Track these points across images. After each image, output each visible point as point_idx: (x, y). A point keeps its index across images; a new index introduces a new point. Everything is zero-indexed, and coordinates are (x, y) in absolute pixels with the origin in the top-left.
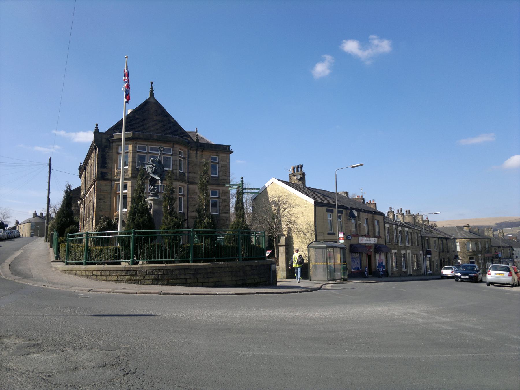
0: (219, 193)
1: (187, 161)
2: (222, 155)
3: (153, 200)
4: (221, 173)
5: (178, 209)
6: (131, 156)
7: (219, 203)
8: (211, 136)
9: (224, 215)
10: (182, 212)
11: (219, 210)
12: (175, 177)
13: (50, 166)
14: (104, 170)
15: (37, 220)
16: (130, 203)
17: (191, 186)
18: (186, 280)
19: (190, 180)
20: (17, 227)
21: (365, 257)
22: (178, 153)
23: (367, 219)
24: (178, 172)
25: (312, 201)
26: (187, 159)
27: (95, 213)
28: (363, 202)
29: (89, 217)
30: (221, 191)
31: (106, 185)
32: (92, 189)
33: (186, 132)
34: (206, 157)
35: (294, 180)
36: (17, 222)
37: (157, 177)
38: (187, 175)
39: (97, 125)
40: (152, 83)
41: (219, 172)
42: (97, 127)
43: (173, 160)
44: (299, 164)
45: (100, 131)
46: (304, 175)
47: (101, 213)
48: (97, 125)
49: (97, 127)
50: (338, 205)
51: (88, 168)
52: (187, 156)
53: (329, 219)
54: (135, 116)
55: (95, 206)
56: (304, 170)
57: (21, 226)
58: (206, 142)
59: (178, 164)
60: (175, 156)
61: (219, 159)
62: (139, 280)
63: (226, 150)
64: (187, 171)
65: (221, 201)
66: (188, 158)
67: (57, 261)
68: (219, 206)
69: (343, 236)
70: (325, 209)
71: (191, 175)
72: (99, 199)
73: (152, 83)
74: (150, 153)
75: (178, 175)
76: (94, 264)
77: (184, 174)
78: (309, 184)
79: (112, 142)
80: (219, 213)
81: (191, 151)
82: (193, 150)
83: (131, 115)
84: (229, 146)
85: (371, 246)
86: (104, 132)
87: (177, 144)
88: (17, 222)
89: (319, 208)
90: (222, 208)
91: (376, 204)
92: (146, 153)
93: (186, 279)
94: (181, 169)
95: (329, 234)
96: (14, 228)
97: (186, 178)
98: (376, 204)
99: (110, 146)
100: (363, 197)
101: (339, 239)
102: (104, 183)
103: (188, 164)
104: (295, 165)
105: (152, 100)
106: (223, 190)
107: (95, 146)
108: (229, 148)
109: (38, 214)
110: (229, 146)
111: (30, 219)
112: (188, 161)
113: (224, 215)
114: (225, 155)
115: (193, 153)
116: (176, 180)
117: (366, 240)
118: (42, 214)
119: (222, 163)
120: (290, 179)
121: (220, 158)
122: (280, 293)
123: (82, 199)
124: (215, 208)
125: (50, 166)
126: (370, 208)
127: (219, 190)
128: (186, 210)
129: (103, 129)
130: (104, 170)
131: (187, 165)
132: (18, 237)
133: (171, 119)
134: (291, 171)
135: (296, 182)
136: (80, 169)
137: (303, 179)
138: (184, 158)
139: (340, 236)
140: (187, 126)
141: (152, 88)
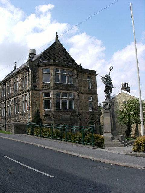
0: (92, 99)
2: (92, 76)
14: (35, 84)
16: (141, 120)
31: (36, 93)
34: (85, 78)
41: (91, 86)
46: (129, 88)
60: (70, 78)
61: (91, 78)
73: (57, 33)
74: (62, 74)
79: (39, 67)
81: (79, 74)
119: (93, 81)
121: (92, 78)
127: (92, 96)
130: (35, 84)
141: (15, 65)
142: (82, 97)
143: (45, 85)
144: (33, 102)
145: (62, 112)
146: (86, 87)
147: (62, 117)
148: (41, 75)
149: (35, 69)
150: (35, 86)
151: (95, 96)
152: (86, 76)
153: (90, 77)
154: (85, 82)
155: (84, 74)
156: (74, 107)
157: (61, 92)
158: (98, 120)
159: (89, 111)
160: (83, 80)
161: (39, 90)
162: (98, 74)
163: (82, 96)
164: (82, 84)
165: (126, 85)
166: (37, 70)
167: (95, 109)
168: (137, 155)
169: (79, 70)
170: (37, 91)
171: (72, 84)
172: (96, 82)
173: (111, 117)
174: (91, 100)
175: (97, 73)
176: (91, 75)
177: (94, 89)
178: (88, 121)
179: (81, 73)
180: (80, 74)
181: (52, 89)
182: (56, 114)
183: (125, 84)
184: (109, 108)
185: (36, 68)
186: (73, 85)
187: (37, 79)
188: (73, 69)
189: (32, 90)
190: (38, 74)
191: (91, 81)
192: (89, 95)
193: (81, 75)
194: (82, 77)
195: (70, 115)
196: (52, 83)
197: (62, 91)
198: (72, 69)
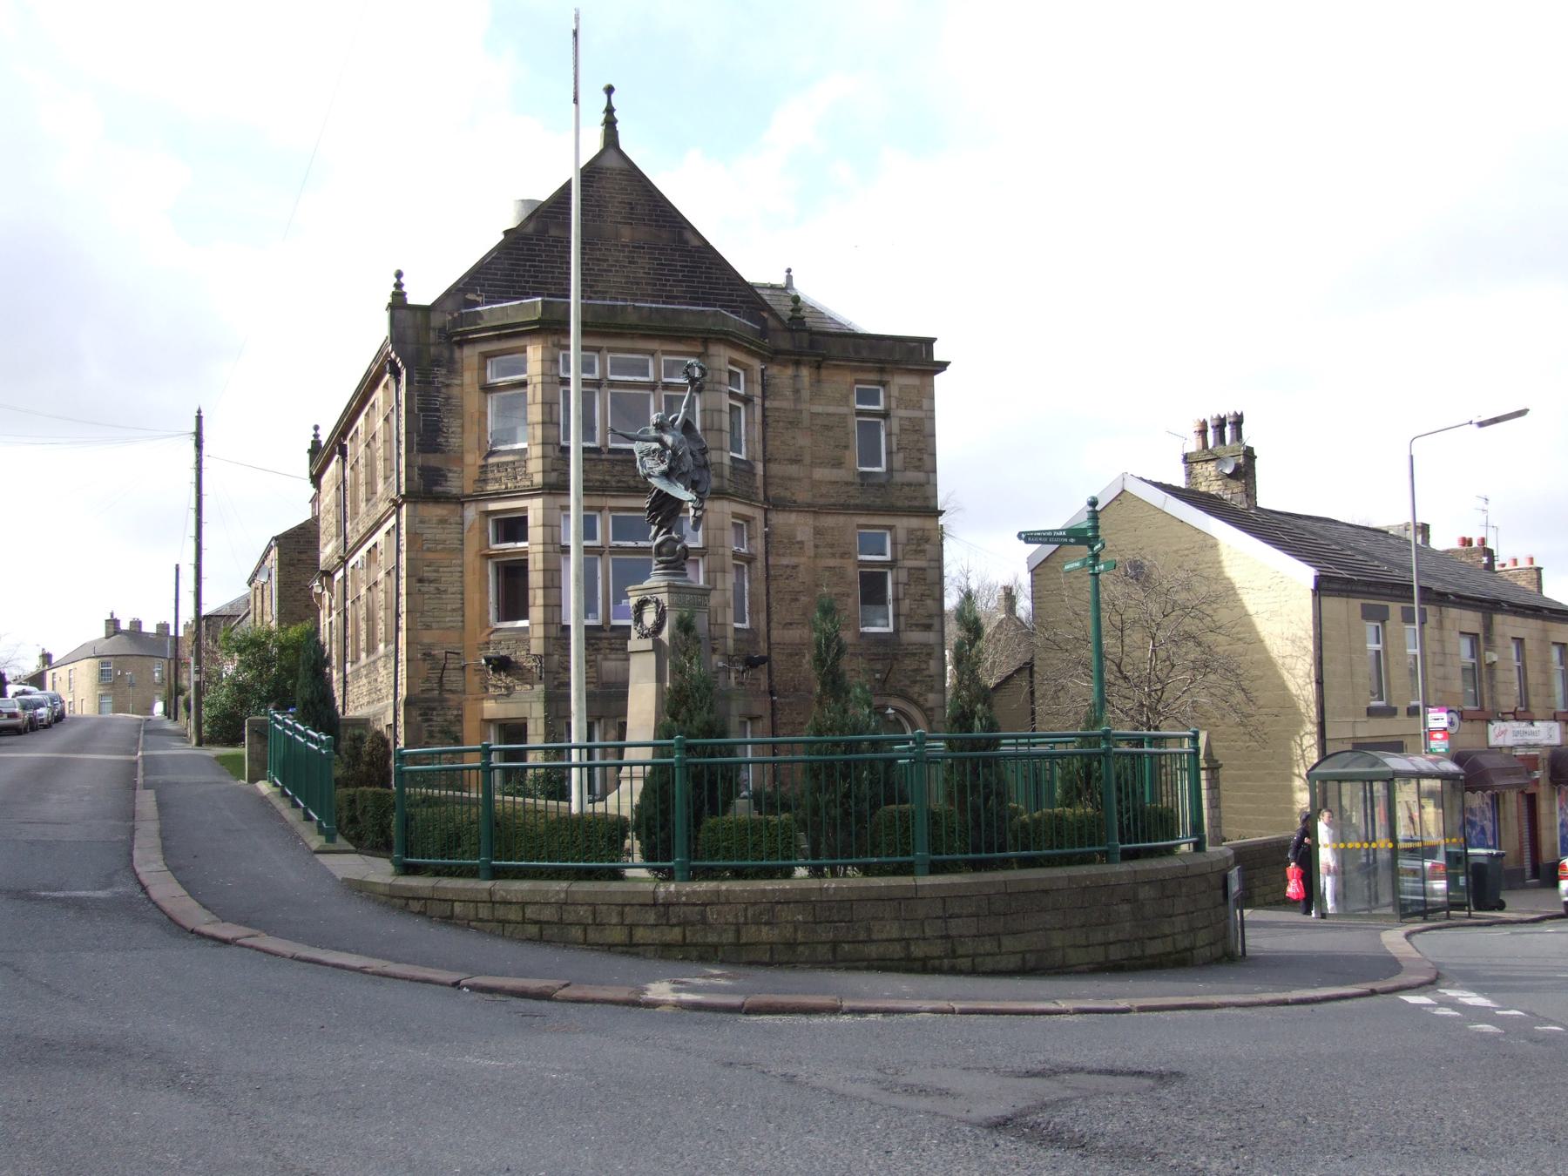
0: (894, 544)
2: (899, 381)
3: (672, 589)
4: (898, 460)
5: (730, 613)
6: (539, 398)
7: (896, 584)
8: (861, 304)
9: (916, 636)
10: (747, 625)
11: (896, 616)
12: (714, 483)
13: (199, 445)
14: (434, 460)
15: (121, 646)
16: (540, 593)
17: (778, 519)
18: (907, 947)
19: (772, 492)
20: (49, 674)
21: (1513, 806)
22: (725, 377)
23: (1520, 641)
24: (727, 461)
25: (1303, 575)
26: (758, 401)
27: (403, 635)
28: (1490, 566)
29: (371, 649)
30: (902, 536)
31: (443, 521)
32: (380, 536)
33: (751, 288)
34: (839, 395)
35: (1210, 480)
36: (47, 658)
37: (680, 492)
38: (759, 468)
39: (399, 275)
40: (609, 90)
41: (889, 453)
42: (399, 285)
43: (703, 411)
44: (1227, 410)
45: (409, 302)
46: (1250, 455)
47: (427, 637)
48: (399, 275)
49: (399, 285)
50: (1421, 588)
51: (356, 448)
52: (758, 390)
53: (1373, 646)
54: (547, 231)
55: (403, 608)
56: (1250, 437)
57: (62, 672)
58: (832, 328)
59: (726, 425)
60: (723, 400)
61: (888, 397)
62: (715, 947)
63: (913, 359)
64: (759, 455)
65: (903, 575)
66: (764, 397)
67: (331, 847)
68: (896, 600)
69: (1444, 724)
70: (1356, 604)
71: (775, 468)
72: (416, 578)
73: (609, 90)
74: (612, 384)
75: (727, 472)
76: (521, 874)
77: (749, 464)
78: (1272, 494)
79: (460, 344)
80: (897, 630)
81: (774, 370)
82: (784, 364)
83: (531, 228)
84: (929, 342)
85: (1535, 758)
86: (428, 301)
87: (719, 341)
88: (47, 658)
89: (1332, 604)
90: (906, 605)
91: (1539, 570)
92: (652, 387)
93: (908, 941)
94: (736, 447)
95: (1371, 712)
96: (37, 680)
97: (759, 482)
98: (1539, 570)
99: (452, 361)
100: (1489, 545)
101: (1430, 734)
102: (435, 511)
103: (765, 424)
104: (1210, 414)
105: (611, 161)
106: (910, 531)
107: (393, 363)
108: (930, 352)
109: (125, 626)
110: (929, 342)
111: (93, 644)
113: (916, 636)
114: (912, 381)
115: (782, 375)
116: (720, 494)
117: (1516, 734)
118: (137, 624)
119: (903, 413)
120: (1189, 474)
121: (895, 391)
122: (1286, 1003)
123: (329, 574)
124: (880, 609)
125: (199, 445)
126: (1515, 587)
127: (890, 528)
128: (763, 616)
129: (423, 293)
130: (434, 460)
131: (758, 429)
132: (59, 718)
133: (688, 235)
134: (1193, 445)
135: (1215, 488)
136: (315, 449)
137: (1245, 471)
138: (747, 400)
139: (1432, 724)
140: (755, 265)
141: (610, 110)
144: (421, 581)
145: (605, 644)
146: (838, 464)
147: (605, 679)
148: (470, 398)
149: (437, 362)
151: (915, 522)
152: (840, 382)
153: (883, 384)
154: (829, 426)
155: (824, 372)
157: (600, 509)
158: (931, 696)
159: (864, 634)
160: (814, 415)
161: (460, 501)
162: (943, 366)
163: (800, 526)
165: (1228, 430)
166: (452, 368)
167: (908, 616)
169: (789, 335)
170: (452, 507)
172: (933, 418)
173: (660, 678)
174: (888, 557)
175: (938, 356)
176: (882, 370)
177: (913, 476)
179: (797, 364)
180: (790, 371)
181: (532, 493)
182: (556, 657)
183: (1220, 424)
184: (659, 626)
185: (446, 354)
187: (453, 425)
189: (406, 498)
190: (455, 391)
191: (885, 415)
192: (863, 520)
193: (796, 377)
194: (806, 394)
196: (536, 451)
197: (613, 503)
198: (700, 349)
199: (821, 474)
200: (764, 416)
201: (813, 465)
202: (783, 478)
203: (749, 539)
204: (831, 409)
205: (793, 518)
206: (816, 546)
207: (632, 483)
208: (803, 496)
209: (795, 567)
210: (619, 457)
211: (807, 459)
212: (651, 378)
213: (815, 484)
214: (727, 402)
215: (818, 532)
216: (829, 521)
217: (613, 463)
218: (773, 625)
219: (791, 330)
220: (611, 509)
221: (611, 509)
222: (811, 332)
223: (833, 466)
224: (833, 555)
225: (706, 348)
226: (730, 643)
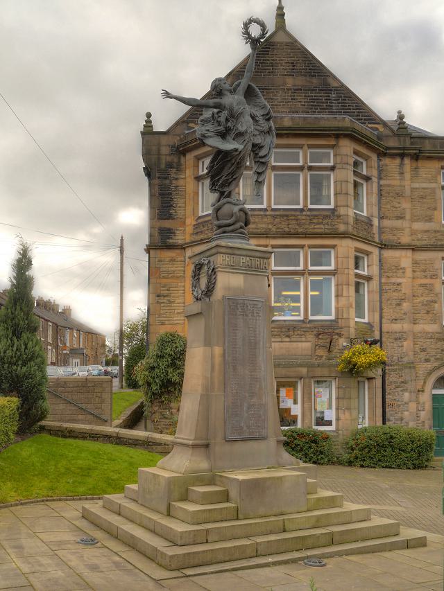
1: (375, 186)
5: (352, 312)
14: (167, 224)
17: (388, 254)
31: (172, 260)
38: (376, 222)
64: (376, 212)
66: (380, 178)
75: (351, 221)
87: (346, 136)
92: (301, 169)
103: (380, 195)
112: (380, 186)
127: (334, 247)
130: (167, 224)
133: (330, 80)
138: (367, 179)
142: (403, 265)
143: (202, 223)
150: (169, 229)
156: (337, 309)
161: (183, 248)
164: (406, 205)
168: (135, 443)
171: (332, 206)
178: (430, 373)
185: (176, 160)
186: (333, 210)
187: (178, 202)
188: (337, 137)
195: (308, 345)
199: (418, 226)
200: (380, 190)
201: (412, 220)
202: (391, 229)
203: (368, 266)
204: (425, 185)
205: (397, 253)
206: (414, 271)
207: (287, 229)
208: (405, 240)
209: (399, 284)
210: (277, 213)
211: (408, 216)
212: (301, 163)
213: (413, 233)
214: (352, 178)
215: (415, 263)
216: (421, 256)
217: (275, 217)
218: (384, 321)
219: (399, 135)
220: (310, 247)
221: (310, 247)
222: (410, 135)
223: (426, 221)
224: (426, 277)
225: (338, 143)
226: (352, 330)
